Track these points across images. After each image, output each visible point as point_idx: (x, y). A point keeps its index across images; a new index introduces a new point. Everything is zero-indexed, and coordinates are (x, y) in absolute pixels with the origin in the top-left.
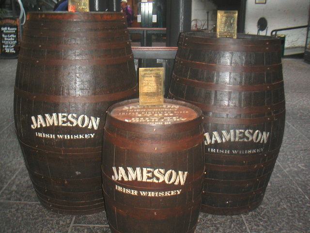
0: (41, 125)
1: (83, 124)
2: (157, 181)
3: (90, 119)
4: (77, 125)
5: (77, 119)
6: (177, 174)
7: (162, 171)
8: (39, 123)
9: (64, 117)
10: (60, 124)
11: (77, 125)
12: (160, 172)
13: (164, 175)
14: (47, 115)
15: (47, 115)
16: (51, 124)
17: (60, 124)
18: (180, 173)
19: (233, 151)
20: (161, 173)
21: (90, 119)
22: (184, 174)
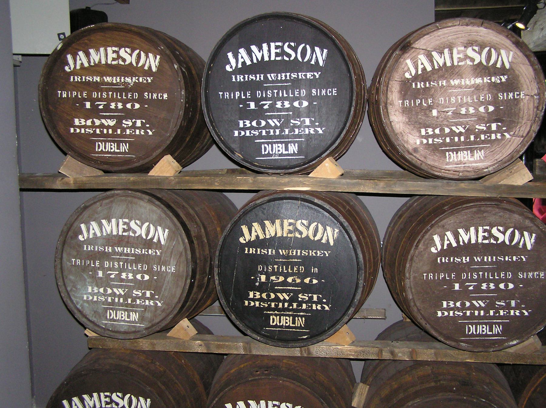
0: (95, 234)
1: (147, 235)
2: (123, 63)
3: (138, 400)
4: (307, 236)
5: (308, 228)
6: (147, 56)
7: (128, 50)
8: (92, 232)
9: (290, 224)
10: (480, 241)
11: (307, 236)
12: (126, 52)
13: (131, 55)
14: (85, 396)
15: (85, 396)
16: (466, 242)
17: (480, 241)
18: (151, 55)
19: (280, 251)
20: (127, 52)
21: (138, 400)
22: (156, 58)
